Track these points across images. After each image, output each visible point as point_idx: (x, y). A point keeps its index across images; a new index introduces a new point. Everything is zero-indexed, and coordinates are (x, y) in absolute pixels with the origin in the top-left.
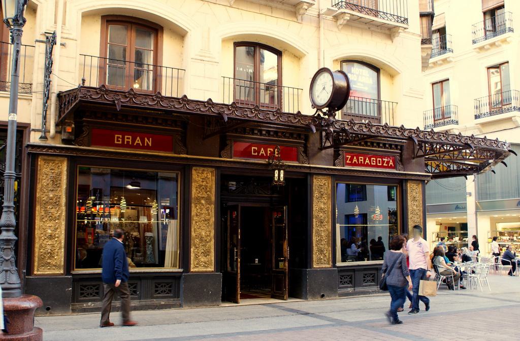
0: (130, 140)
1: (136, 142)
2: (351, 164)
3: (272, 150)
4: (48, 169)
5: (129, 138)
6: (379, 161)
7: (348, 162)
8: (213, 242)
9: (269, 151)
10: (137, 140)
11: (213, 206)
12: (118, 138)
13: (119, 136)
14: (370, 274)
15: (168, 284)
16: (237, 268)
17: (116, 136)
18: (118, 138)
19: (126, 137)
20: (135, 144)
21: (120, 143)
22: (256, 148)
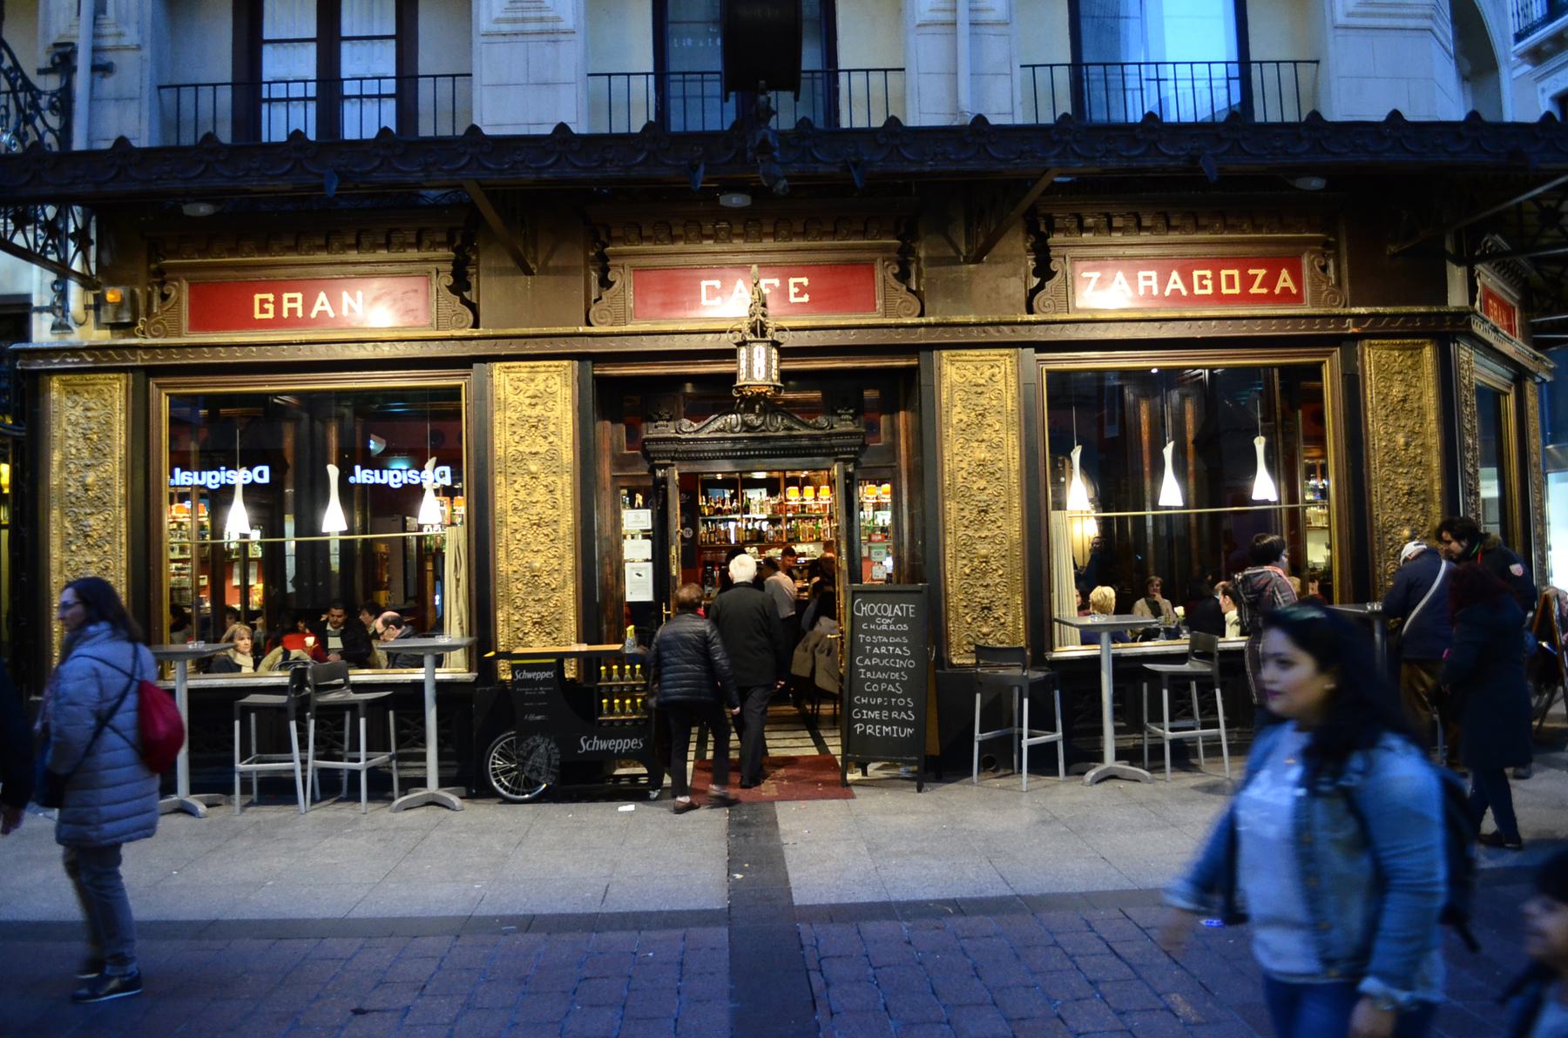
3: (776, 282)
4: (79, 411)
5: (1149, 278)
8: (570, 588)
9: (796, 285)
11: (567, 478)
13: (264, 296)
16: (1021, 725)
19: (286, 296)
22: (805, 281)
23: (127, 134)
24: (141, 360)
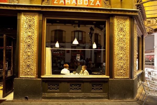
10: (97, 2)
14: (98, 84)
20: (60, 3)
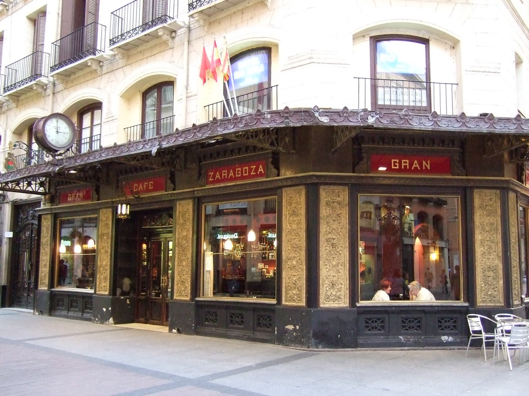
0: (407, 164)
1: (414, 166)
2: (214, 182)
5: (406, 162)
6: (246, 170)
7: (210, 180)
12: (395, 162)
15: (452, 320)
17: (393, 160)
18: (395, 162)
19: (403, 161)
20: (413, 168)
21: (398, 167)
23: (195, 123)
24: (353, 181)
